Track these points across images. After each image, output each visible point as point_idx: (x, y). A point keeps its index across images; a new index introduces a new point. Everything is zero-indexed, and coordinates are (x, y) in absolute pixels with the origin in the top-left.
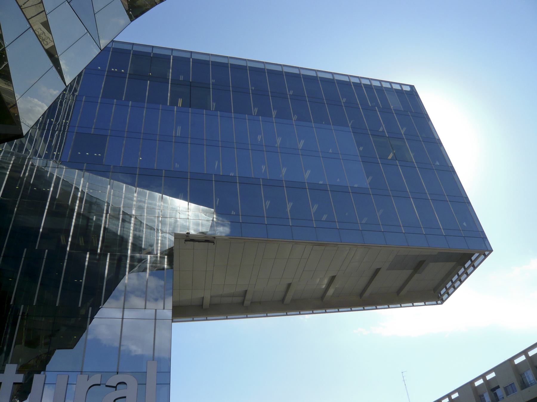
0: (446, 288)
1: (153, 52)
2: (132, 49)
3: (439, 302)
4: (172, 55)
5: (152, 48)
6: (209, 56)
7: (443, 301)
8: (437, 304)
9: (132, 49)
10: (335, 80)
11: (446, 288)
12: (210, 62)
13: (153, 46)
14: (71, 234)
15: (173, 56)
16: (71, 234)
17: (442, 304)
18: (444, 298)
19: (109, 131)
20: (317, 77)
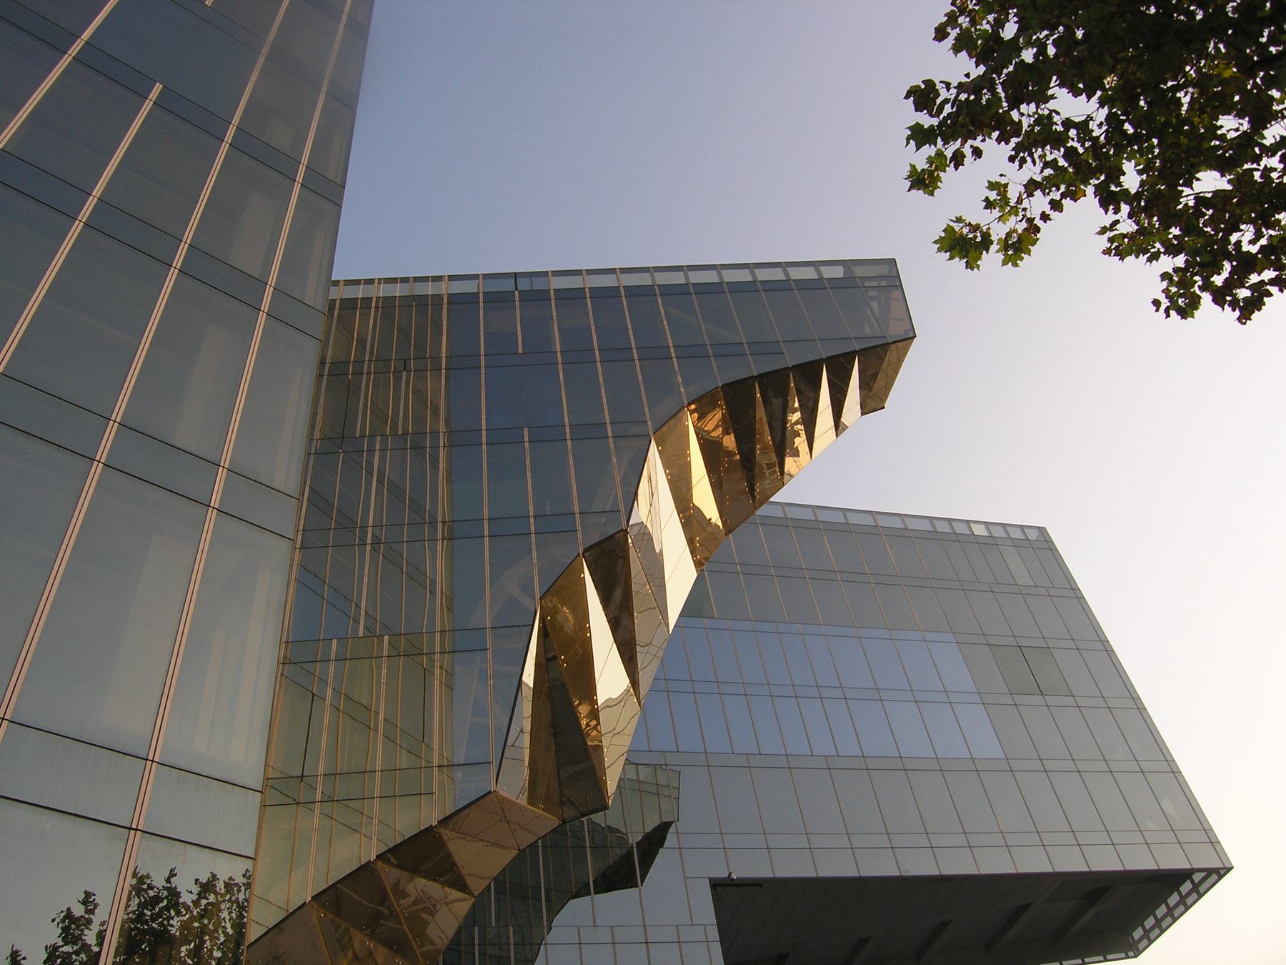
0: (1144, 928)
1: (519, 288)
2: (516, 287)
3: (1131, 954)
4: (516, 289)
5: (513, 281)
6: (615, 276)
7: (1138, 953)
8: (1128, 957)
9: (516, 287)
10: (791, 282)
11: (1144, 928)
12: (587, 290)
13: (515, 273)
14: (642, 389)
15: (519, 291)
16: (642, 389)
17: (1136, 956)
18: (1141, 946)
19: (377, 793)
20: (788, 280)
